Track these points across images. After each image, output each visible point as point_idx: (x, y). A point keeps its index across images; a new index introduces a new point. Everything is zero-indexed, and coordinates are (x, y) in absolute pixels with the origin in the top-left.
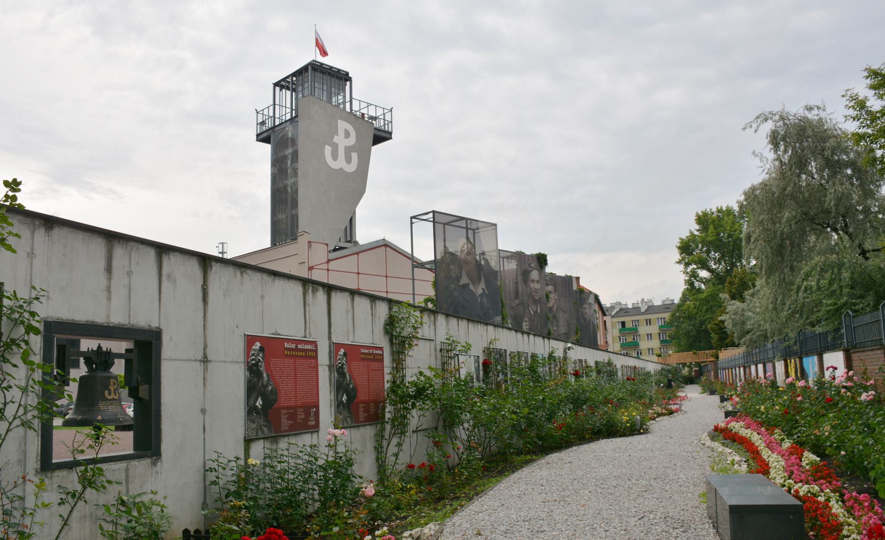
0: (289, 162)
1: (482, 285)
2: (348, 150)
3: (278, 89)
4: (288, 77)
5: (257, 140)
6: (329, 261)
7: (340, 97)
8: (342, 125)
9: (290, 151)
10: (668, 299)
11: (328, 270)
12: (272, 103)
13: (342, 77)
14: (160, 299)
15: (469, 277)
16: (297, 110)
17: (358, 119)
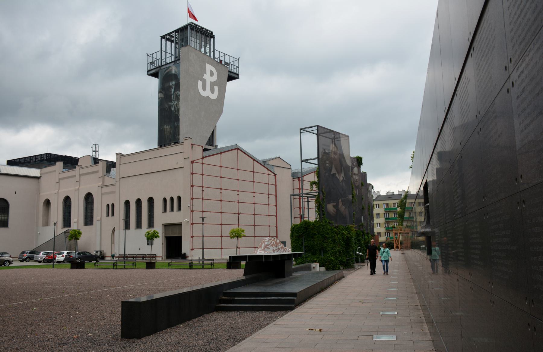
0: (173, 90)
1: (343, 175)
2: (213, 84)
4: (172, 32)
6: (203, 158)
8: (209, 67)
9: (174, 83)
10: (390, 192)
11: (203, 164)
12: (159, 49)
13: (208, 35)
15: (336, 169)
17: (220, 64)
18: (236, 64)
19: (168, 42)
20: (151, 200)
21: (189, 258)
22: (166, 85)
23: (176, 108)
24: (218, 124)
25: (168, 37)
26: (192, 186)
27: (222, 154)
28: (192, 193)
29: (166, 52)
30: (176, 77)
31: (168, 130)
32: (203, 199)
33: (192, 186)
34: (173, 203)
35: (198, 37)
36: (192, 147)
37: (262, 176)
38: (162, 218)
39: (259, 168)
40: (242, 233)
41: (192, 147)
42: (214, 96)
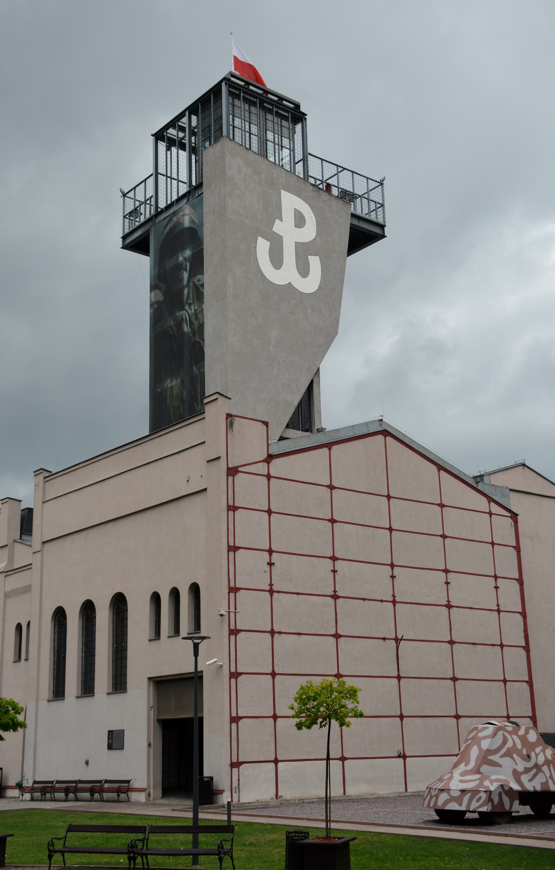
0: (186, 275)
2: (303, 251)
3: (162, 146)
5: (123, 248)
6: (270, 458)
8: (290, 202)
9: (188, 253)
11: (269, 477)
12: (151, 171)
16: (200, 175)
18: (376, 195)
20: (119, 603)
21: (225, 798)
22: (170, 264)
23: (196, 323)
26: (233, 549)
27: (334, 448)
28: (232, 570)
30: (193, 237)
31: (176, 391)
32: (271, 592)
33: (233, 549)
34: (181, 608)
35: (254, 118)
36: (230, 425)
37: (470, 519)
38: (153, 656)
39: (455, 492)
40: (350, 704)
41: (230, 425)
42: (310, 284)
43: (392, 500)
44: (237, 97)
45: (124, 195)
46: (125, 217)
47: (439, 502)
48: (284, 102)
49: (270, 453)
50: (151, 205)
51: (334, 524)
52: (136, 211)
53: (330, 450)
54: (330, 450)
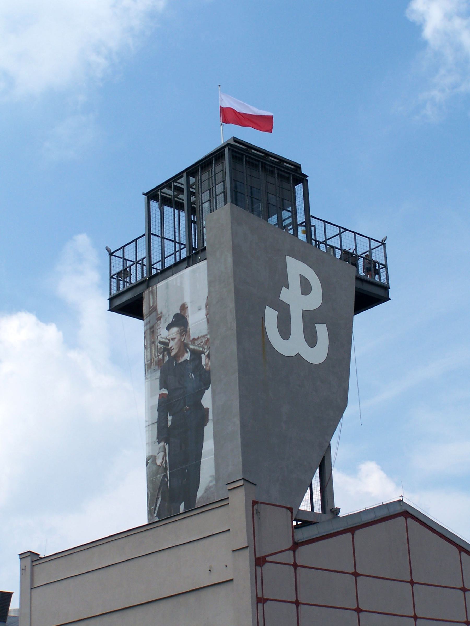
2: (310, 319)
4: (179, 176)
5: (112, 309)
6: (296, 545)
7: (286, 214)
8: (296, 268)
11: (295, 566)
12: (143, 230)
14: (31, 600)
18: (377, 256)
19: (168, 210)
24: (333, 442)
25: (168, 192)
27: (357, 532)
29: (163, 238)
42: (317, 355)
43: (415, 586)
44: (241, 160)
45: (111, 254)
46: (111, 277)
47: (461, 586)
48: (285, 164)
49: (296, 539)
50: (143, 265)
51: (360, 614)
52: (126, 272)
53: (353, 535)
54: (353, 535)
